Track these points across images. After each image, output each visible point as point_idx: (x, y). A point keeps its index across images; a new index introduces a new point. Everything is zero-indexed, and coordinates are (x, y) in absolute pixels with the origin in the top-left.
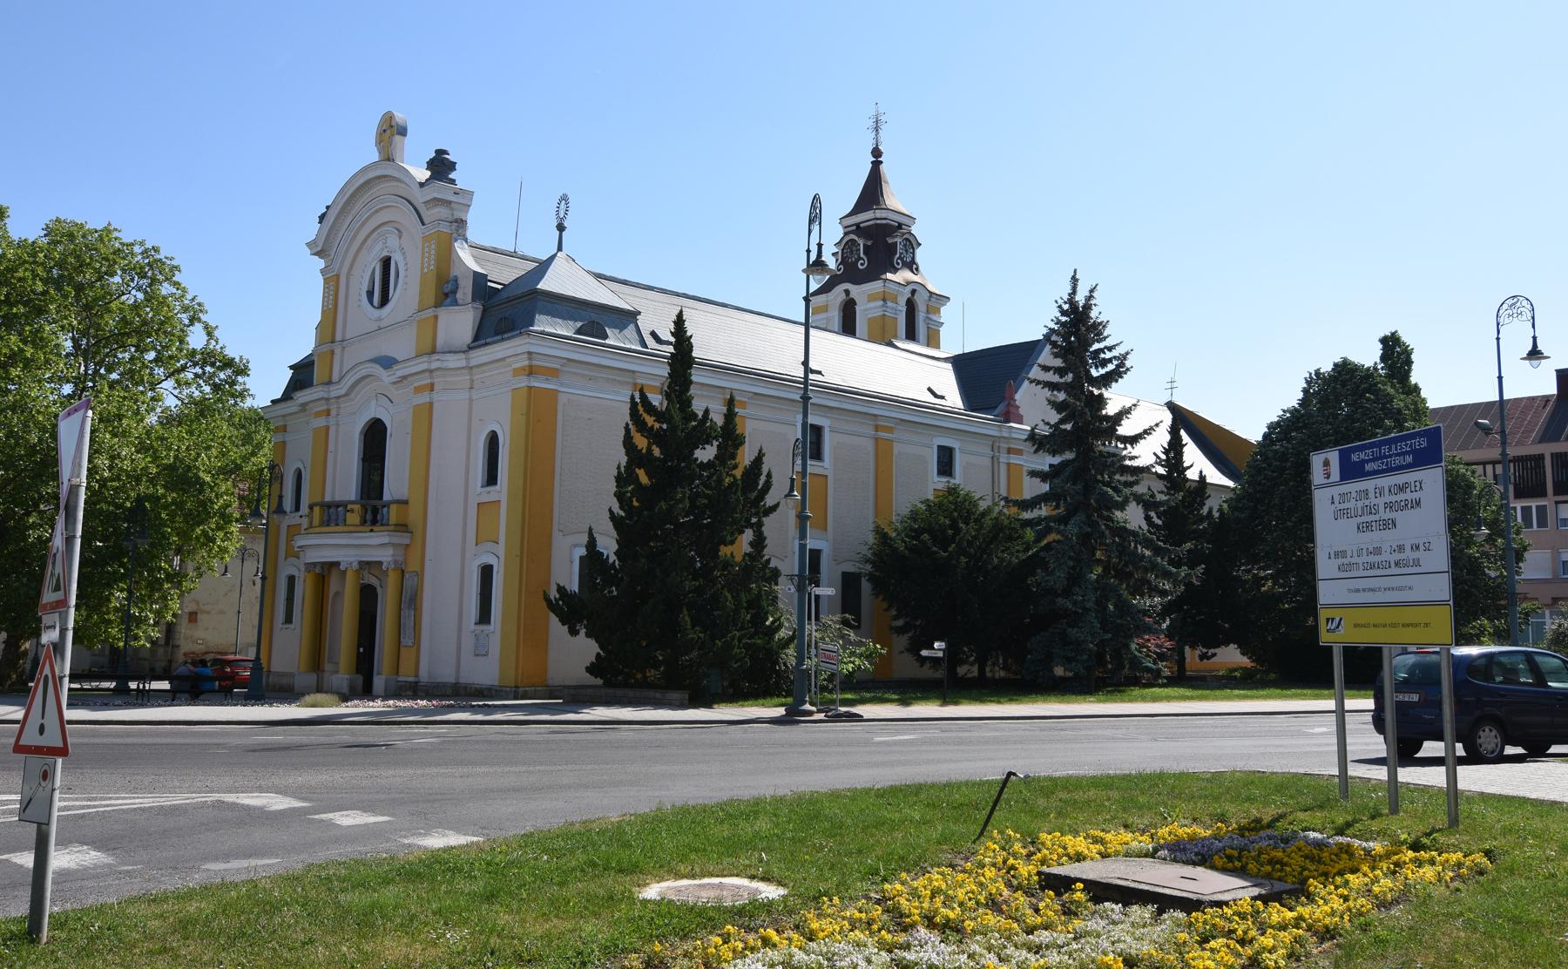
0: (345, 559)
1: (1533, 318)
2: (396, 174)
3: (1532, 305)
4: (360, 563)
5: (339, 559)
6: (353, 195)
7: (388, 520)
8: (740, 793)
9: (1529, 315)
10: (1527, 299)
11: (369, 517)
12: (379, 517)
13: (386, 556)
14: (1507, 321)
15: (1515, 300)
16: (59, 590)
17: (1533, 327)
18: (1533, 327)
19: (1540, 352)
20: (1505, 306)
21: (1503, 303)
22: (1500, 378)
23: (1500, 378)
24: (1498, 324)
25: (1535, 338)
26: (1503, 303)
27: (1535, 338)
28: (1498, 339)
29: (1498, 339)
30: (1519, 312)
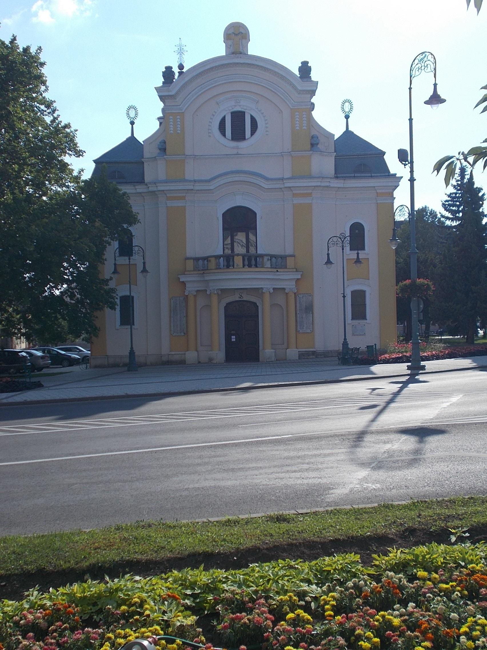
0: (265, 287)
1: (435, 69)
2: (249, 62)
3: (434, 58)
4: (274, 289)
5: (284, 287)
6: (212, 69)
7: (208, 267)
8: (139, 557)
9: (433, 67)
10: (432, 54)
11: (246, 263)
12: (231, 263)
13: (290, 286)
14: (417, 73)
15: (424, 55)
16: (353, 293)
17: (435, 77)
18: (435, 77)
19: (439, 96)
20: (416, 61)
21: (415, 59)
22: (411, 120)
23: (411, 120)
24: (411, 77)
25: (435, 85)
26: (415, 59)
27: (435, 85)
28: (410, 89)
29: (410, 89)
30: (426, 65)
